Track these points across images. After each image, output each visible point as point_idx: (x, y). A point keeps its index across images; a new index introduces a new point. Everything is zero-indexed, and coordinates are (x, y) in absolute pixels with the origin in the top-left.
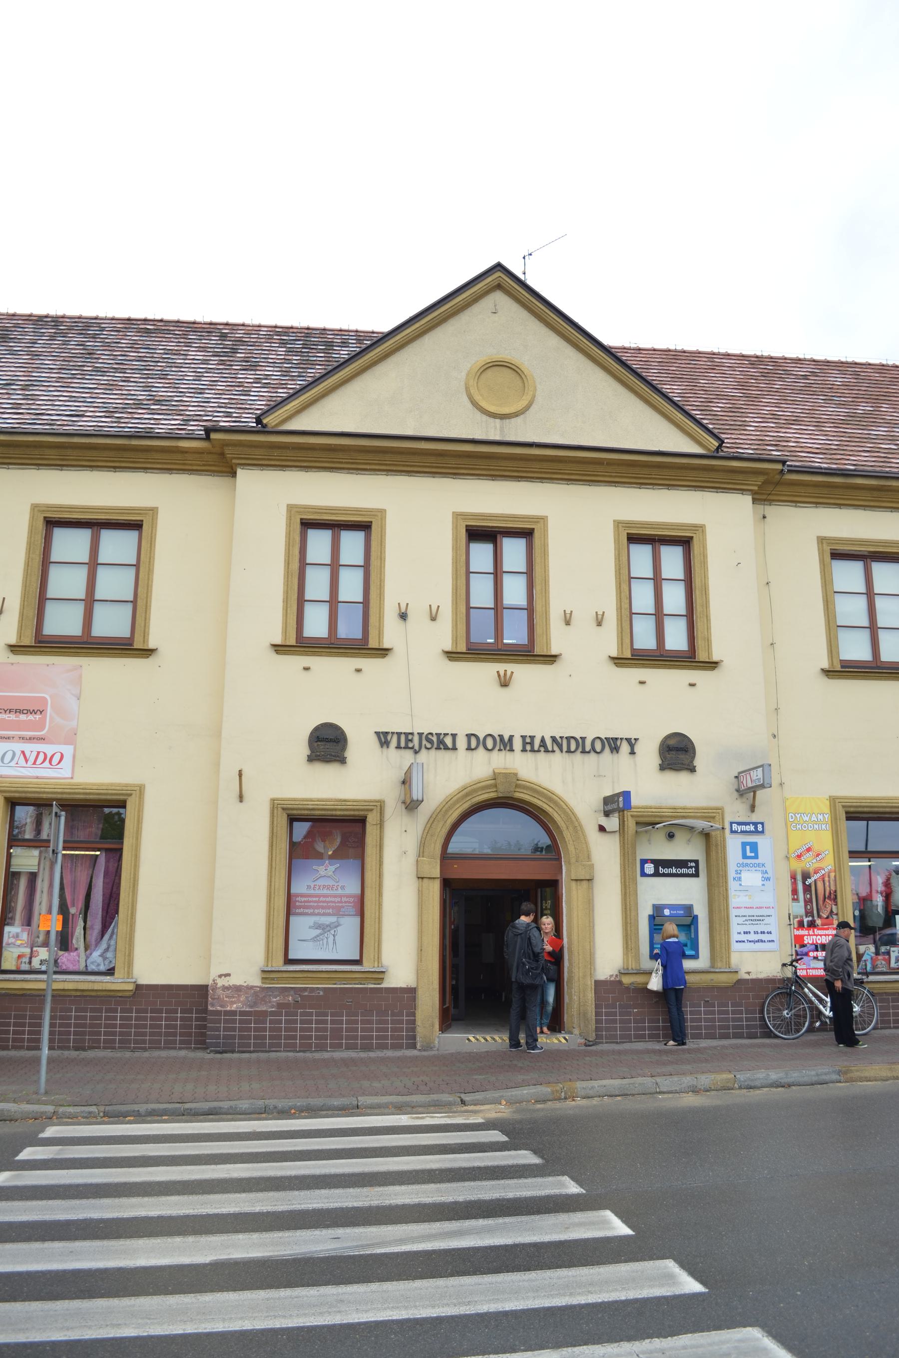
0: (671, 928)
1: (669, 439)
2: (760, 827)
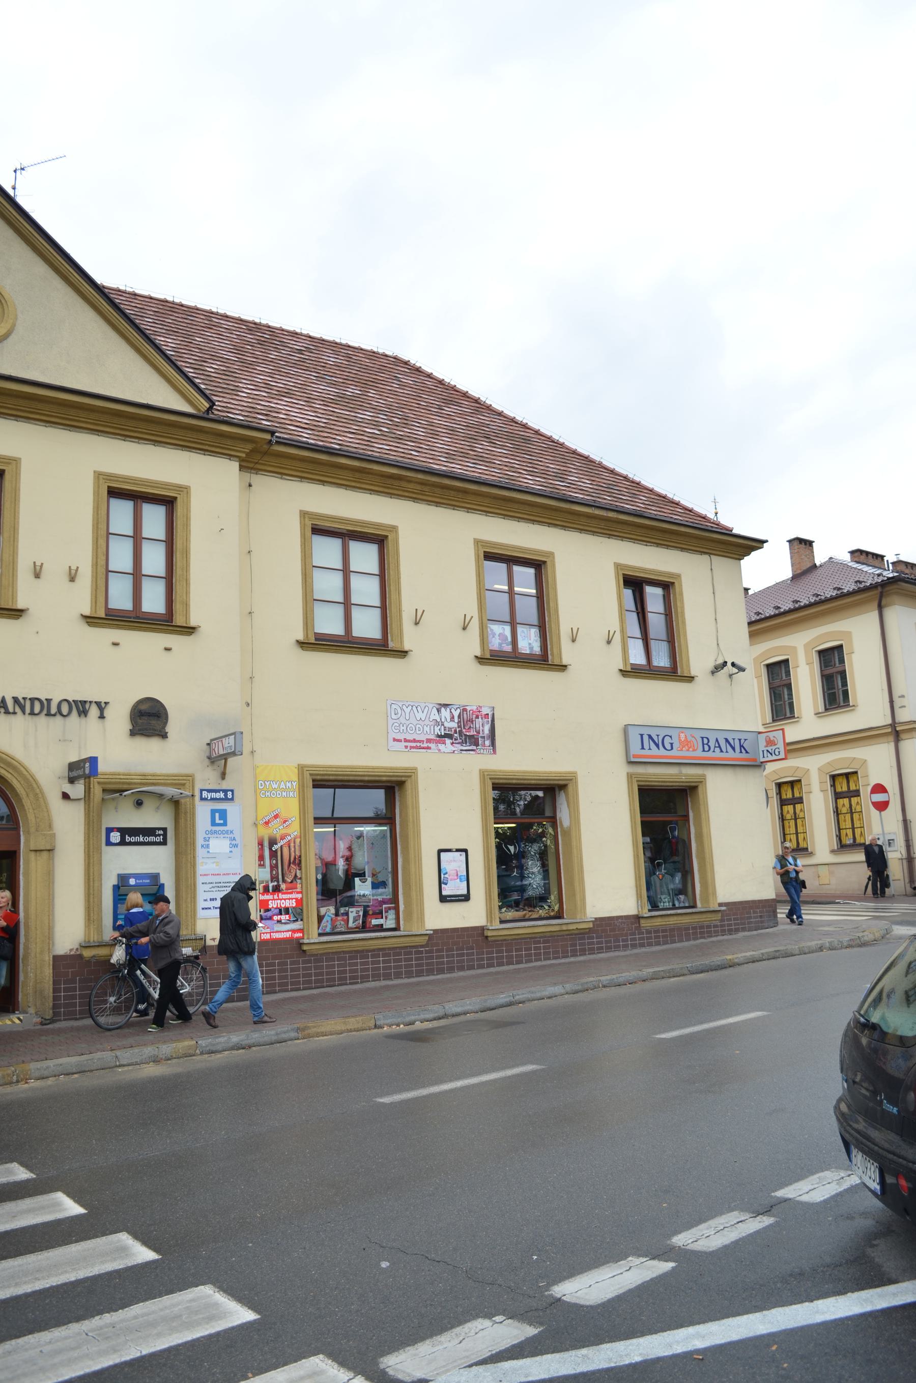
0: (135, 897)
1: (159, 393)
2: (230, 795)
